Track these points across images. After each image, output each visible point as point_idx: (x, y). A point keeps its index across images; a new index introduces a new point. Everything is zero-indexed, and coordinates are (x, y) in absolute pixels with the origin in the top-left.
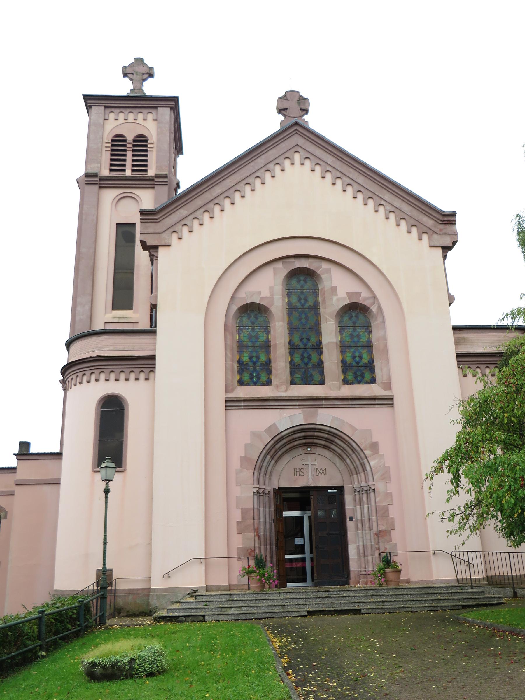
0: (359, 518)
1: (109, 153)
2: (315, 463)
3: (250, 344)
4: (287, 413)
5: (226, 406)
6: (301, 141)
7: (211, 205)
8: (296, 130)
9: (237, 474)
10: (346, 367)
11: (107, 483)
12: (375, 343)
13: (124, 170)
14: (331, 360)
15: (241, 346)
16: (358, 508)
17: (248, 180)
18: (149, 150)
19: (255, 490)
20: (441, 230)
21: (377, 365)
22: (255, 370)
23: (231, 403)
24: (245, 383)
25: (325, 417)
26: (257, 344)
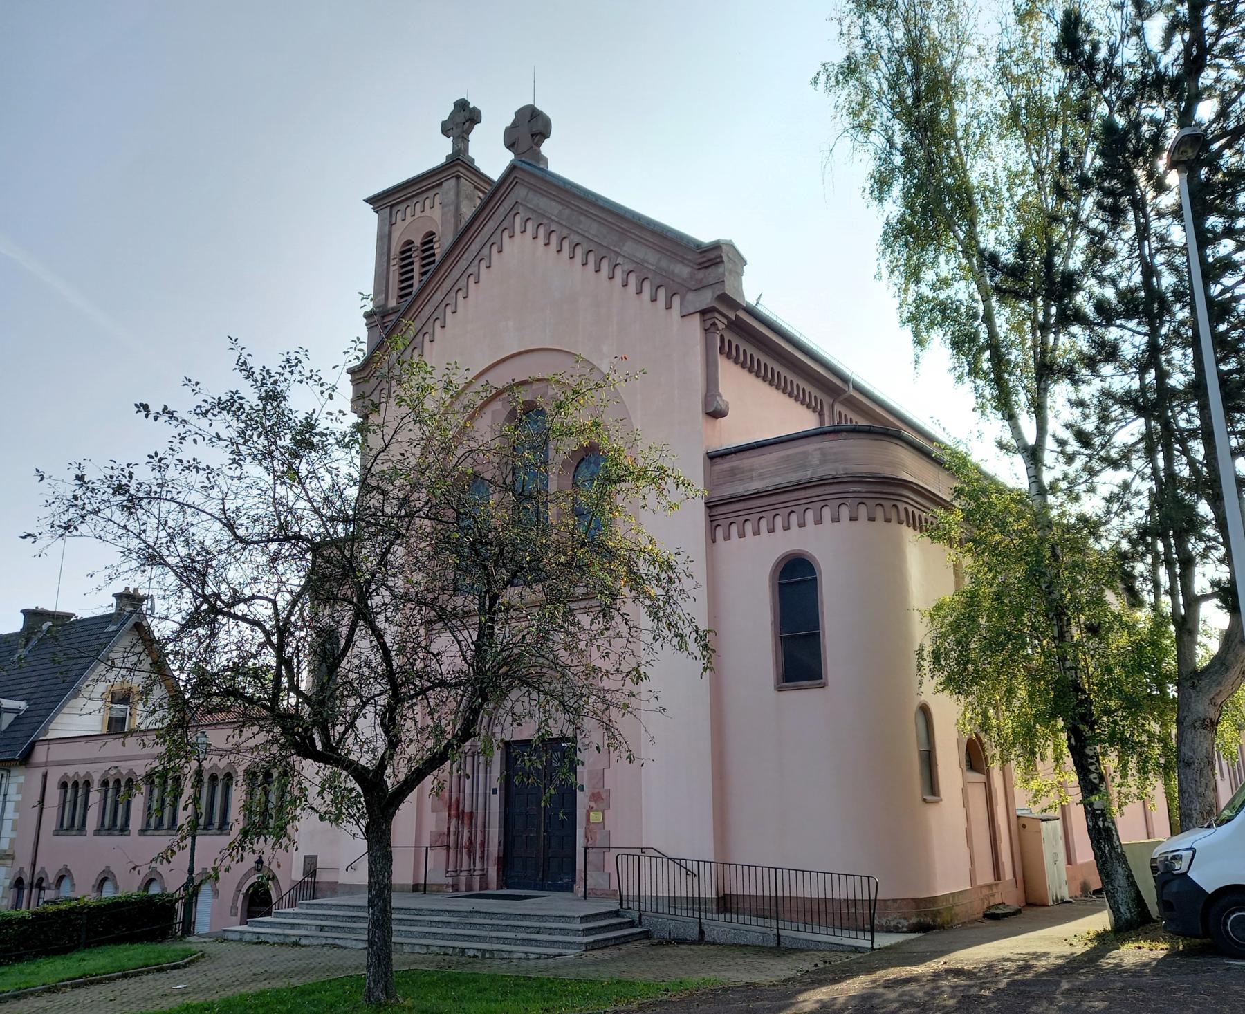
20: (701, 281)
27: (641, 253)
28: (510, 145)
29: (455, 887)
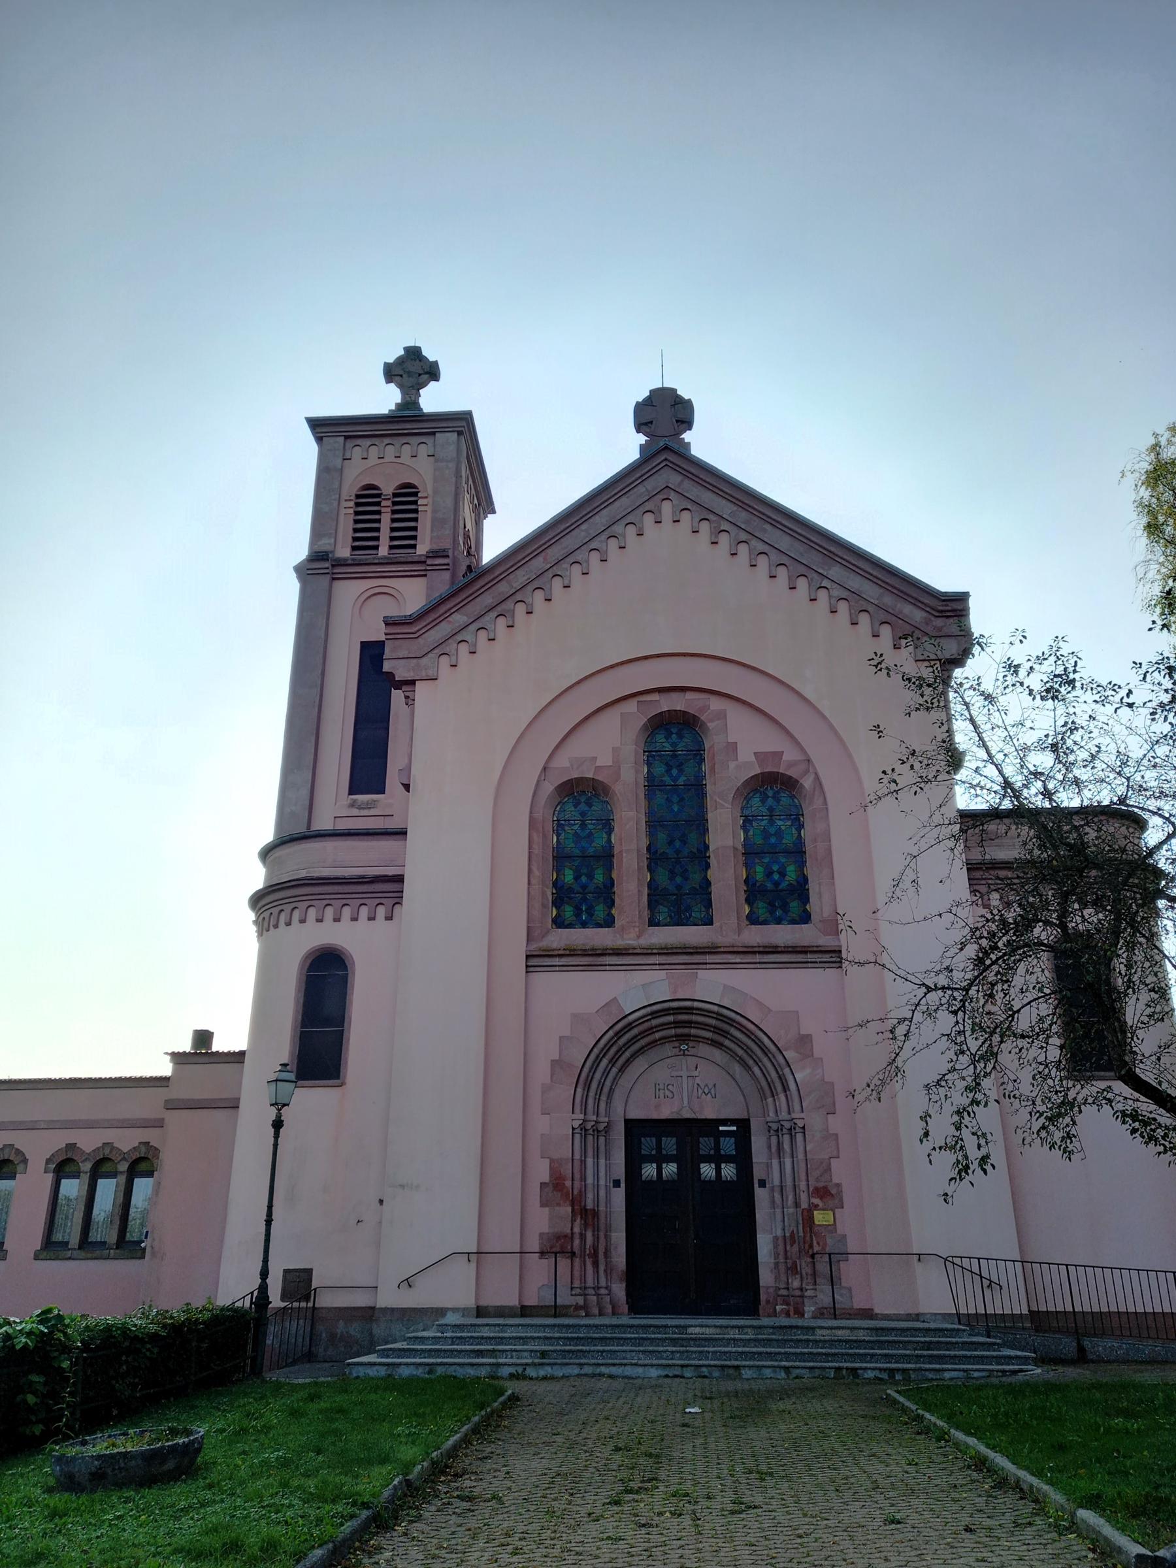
0: (777, 1182)
1: (352, 517)
2: (696, 1073)
3: (577, 852)
4: (639, 978)
5: (527, 966)
6: (674, 479)
7: (509, 605)
8: (666, 459)
9: (543, 1093)
10: (753, 892)
11: (279, 1110)
12: (809, 847)
13: (376, 548)
14: (726, 878)
15: (560, 858)
16: (775, 1162)
17: (578, 556)
18: (420, 509)
19: (576, 1124)
20: (940, 629)
21: (813, 887)
22: (584, 900)
23: (537, 960)
24: (566, 923)
25: (712, 986)
26: (591, 851)
27: (855, 582)
28: (640, 427)
29: (585, 1307)
